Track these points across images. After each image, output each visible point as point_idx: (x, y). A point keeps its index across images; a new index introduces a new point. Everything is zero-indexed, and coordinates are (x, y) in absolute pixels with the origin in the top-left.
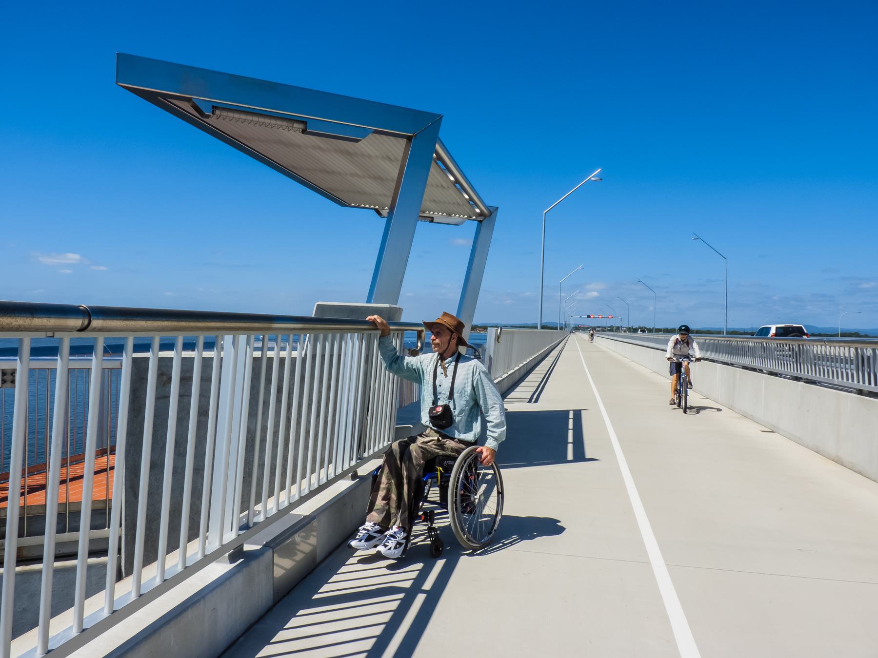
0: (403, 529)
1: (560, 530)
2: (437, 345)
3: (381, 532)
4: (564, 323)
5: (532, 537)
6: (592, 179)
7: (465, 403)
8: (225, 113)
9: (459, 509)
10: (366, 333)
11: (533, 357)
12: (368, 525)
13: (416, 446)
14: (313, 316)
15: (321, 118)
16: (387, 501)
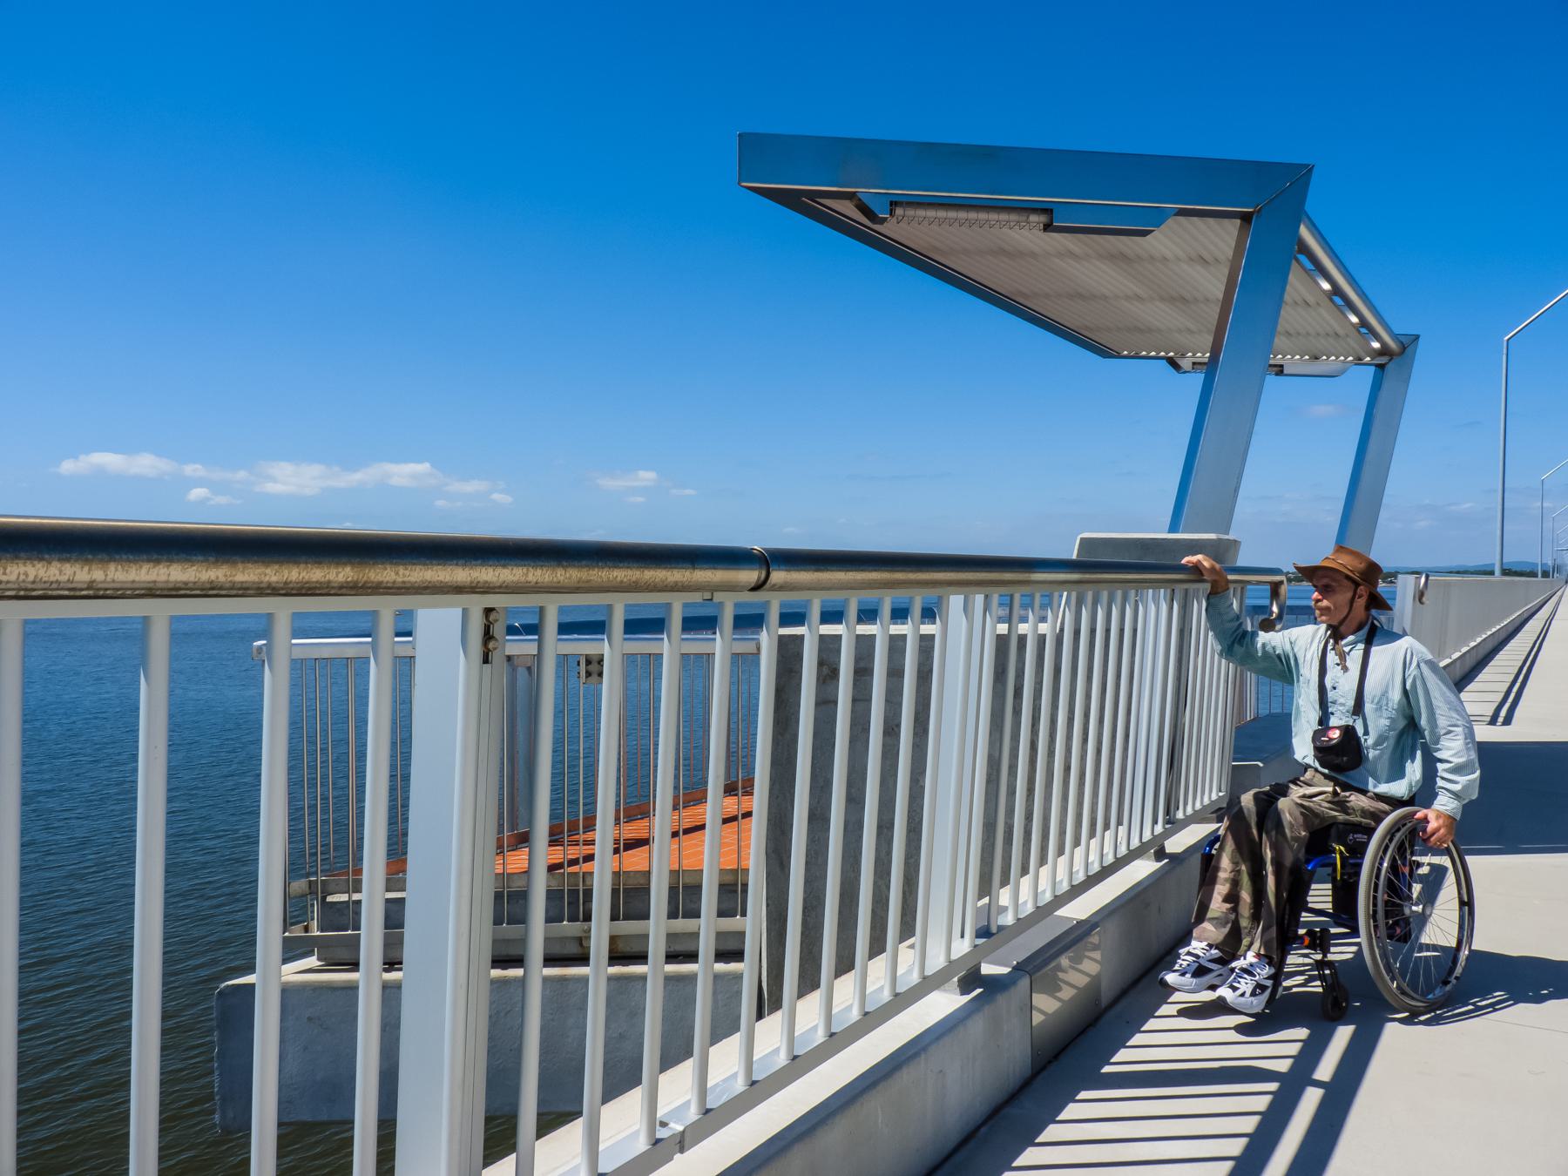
0: (1267, 960)
2: (1325, 611)
4: (1550, 563)
5: (1538, 999)
7: (1387, 722)
8: (910, 212)
9: (1383, 930)
10: (1179, 588)
11: (1489, 633)
12: (1197, 946)
15: (1032, 196)
16: (1232, 905)
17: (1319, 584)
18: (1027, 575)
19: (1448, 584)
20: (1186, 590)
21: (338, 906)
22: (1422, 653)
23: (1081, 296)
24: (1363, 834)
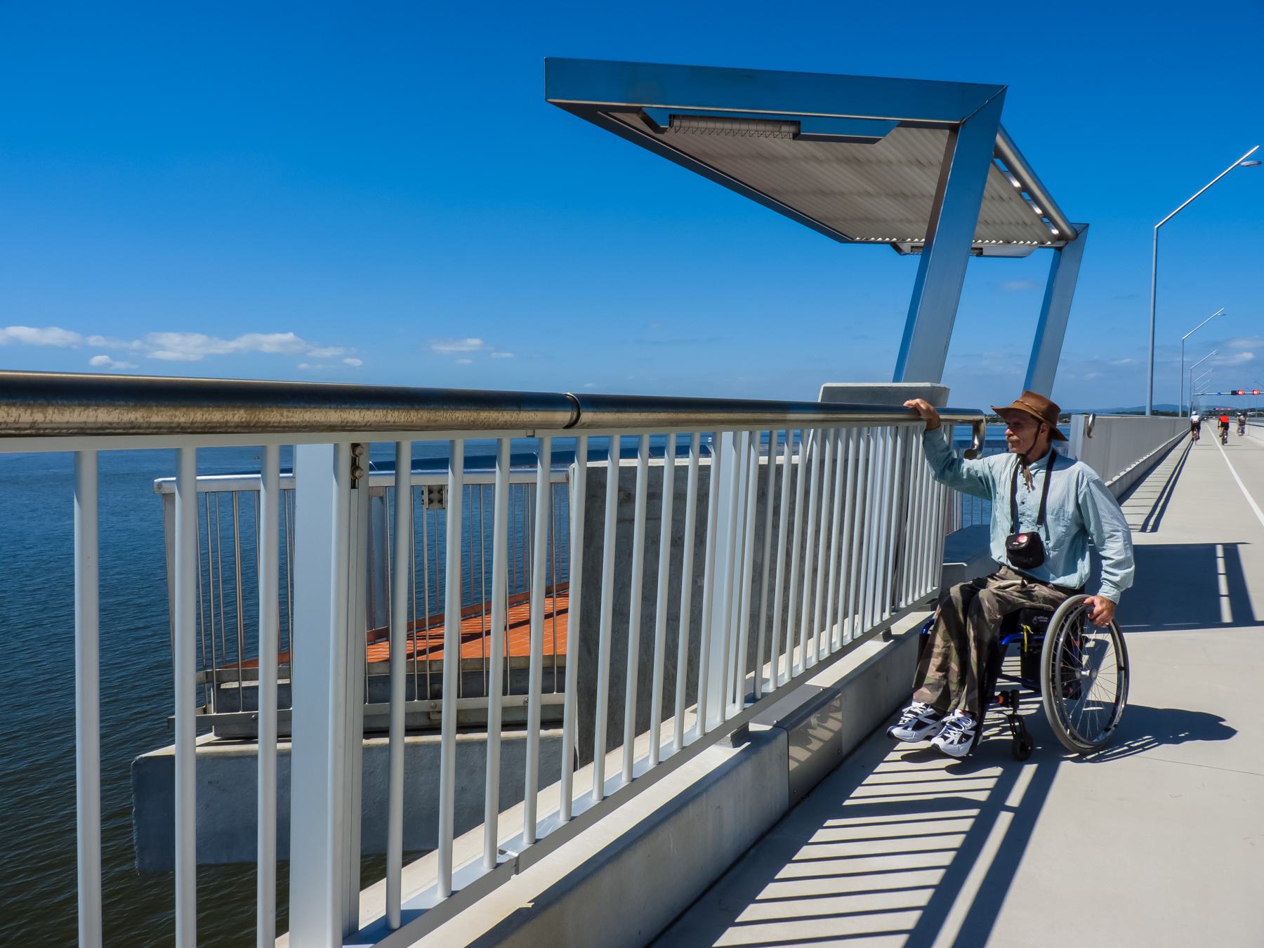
0: (970, 716)
1: (1228, 733)
2: (1015, 443)
3: (937, 717)
4: (1188, 405)
5: (1178, 741)
6: (1243, 164)
7: (1063, 529)
8: (686, 124)
11: (1141, 460)
12: (916, 706)
13: (989, 593)
14: (819, 401)
16: (944, 673)
18: (783, 415)
21: (231, 692)
22: (1091, 474)
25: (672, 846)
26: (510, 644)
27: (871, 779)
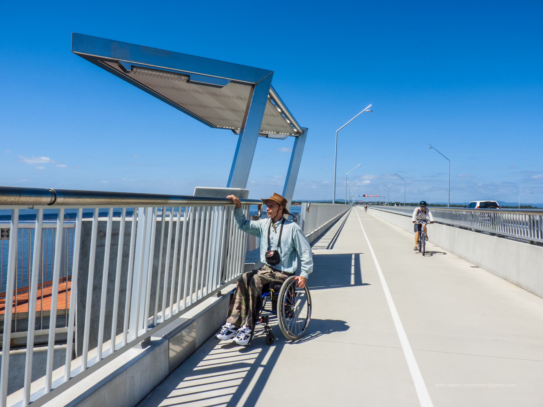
0: (249, 328)
2: (270, 213)
3: (236, 329)
4: (349, 200)
5: (329, 332)
6: (367, 111)
7: (287, 249)
8: (139, 70)
9: (284, 315)
11: (330, 221)
12: (228, 325)
14: (194, 195)
16: (239, 310)
17: (269, 205)
18: (166, 201)
19: (317, 206)
20: (229, 207)
22: (298, 227)
23: (203, 107)
24: (280, 285)
25: (107, 397)
26: (28, 308)
27: (207, 358)
